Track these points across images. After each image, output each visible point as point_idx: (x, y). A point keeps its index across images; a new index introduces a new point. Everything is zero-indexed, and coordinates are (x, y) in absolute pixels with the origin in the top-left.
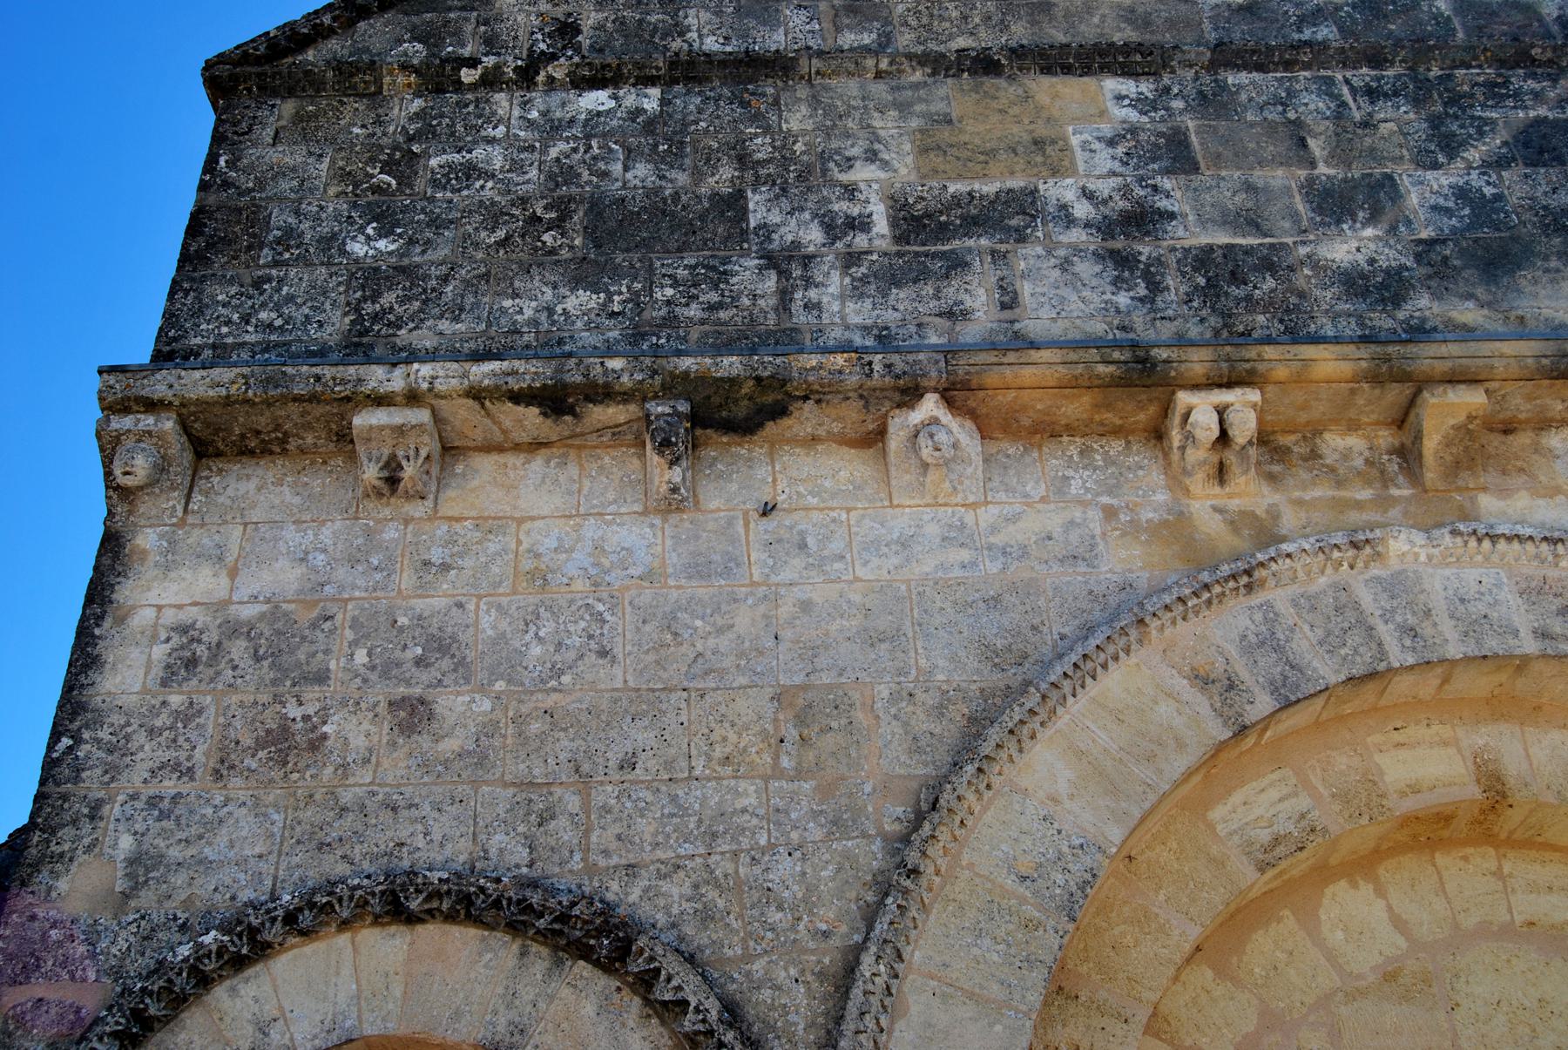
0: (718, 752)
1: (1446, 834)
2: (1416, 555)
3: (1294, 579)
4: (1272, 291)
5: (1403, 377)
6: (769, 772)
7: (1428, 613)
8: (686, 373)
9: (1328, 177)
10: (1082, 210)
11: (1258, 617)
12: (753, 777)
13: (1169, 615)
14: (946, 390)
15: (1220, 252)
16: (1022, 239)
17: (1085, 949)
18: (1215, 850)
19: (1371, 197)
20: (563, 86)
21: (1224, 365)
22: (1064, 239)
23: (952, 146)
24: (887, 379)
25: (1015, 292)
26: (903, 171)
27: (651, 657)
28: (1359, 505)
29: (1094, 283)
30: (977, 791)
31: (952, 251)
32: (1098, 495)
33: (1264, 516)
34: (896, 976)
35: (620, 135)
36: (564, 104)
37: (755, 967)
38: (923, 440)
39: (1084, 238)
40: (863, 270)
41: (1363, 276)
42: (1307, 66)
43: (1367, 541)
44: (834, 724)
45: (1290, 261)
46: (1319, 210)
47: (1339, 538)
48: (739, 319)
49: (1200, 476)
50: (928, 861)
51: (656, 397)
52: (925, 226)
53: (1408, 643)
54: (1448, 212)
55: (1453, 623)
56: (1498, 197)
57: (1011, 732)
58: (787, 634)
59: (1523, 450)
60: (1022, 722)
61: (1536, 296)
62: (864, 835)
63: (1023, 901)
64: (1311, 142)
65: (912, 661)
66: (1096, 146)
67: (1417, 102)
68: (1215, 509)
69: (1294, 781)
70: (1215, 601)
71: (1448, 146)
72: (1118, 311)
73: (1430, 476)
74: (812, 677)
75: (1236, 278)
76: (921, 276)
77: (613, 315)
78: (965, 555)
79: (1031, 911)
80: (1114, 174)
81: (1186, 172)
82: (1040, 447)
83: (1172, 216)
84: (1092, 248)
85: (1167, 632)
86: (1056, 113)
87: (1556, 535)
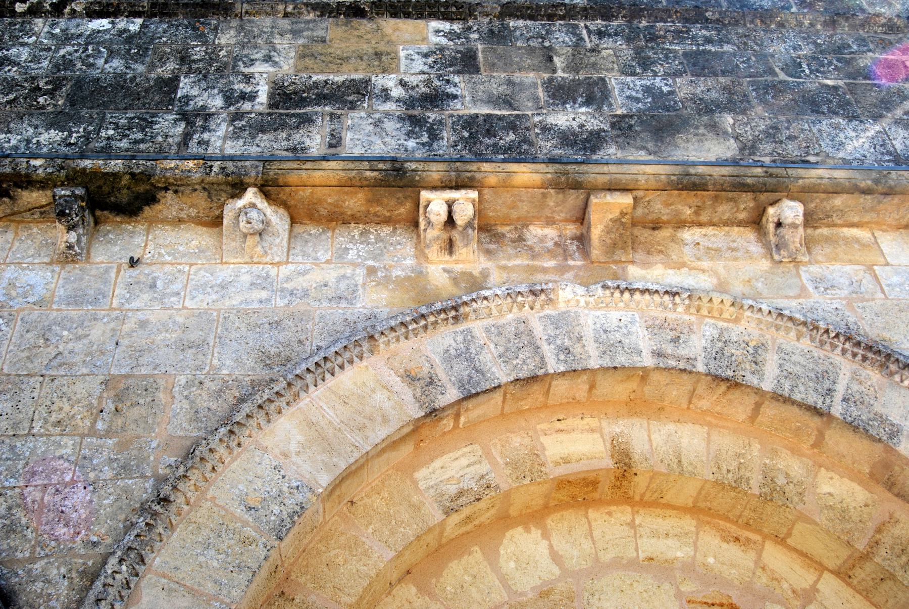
0: (54, 418)
1: (596, 495)
2: (578, 301)
3: (490, 315)
4: (512, 141)
5: (576, 186)
6: (86, 432)
7: (580, 339)
8: (84, 169)
9: (563, 78)
10: (397, 92)
11: (460, 338)
12: (74, 435)
13: (394, 334)
14: (263, 185)
15: (482, 118)
16: (353, 106)
17: (307, 566)
18: (415, 499)
19: (595, 94)
20: (81, 16)
21: (453, 174)
22: (381, 108)
23: (321, 54)
24: (220, 176)
25: (341, 138)
26: (286, 67)
27: (26, 354)
28: (545, 270)
29: (394, 134)
30: (228, 447)
31: (304, 113)
32: (366, 259)
33: (478, 275)
34: (137, 575)
35: (108, 44)
36: (78, 26)
37: (36, 566)
38: (242, 218)
39: (394, 107)
40: (244, 123)
41: (574, 134)
42: (562, 18)
43: (542, 290)
44: (142, 401)
45: (528, 124)
46: (553, 96)
47: (523, 288)
48: (152, 149)
49: (435, 247)
50: (179, 494)
51: (62, 185)
52: (291, 99)
53: (562, 357)
54: (638, 100)
55: (597, 345)
56: (671, 93)
57: (260, 407)
58: (125, 342)
59: (664, 239)
60: (270, 401)
61: (687, 149)
62: (143, 476)
63: (246, 524)
64: (556, 59)
65: (209, 361)
66: (416, 57)
67: (629, 40)
68: (445, 270)
69: (480, 453)
70: (430, 327)
71: (644, 63)
72: (406, 150)
73: (596, 252)
74: (134, 370)
75: (489, 133)
76: (282, 126)
77: (70, 144)
78: (264, 294)
79: (249, 532)
80: (424, 73)
81: (470, 73)
82: (334, 230)
83: (455, 97)
84: (398, 113)
85: (392, 346)
86: (394, 38)
87: (674, 290)
